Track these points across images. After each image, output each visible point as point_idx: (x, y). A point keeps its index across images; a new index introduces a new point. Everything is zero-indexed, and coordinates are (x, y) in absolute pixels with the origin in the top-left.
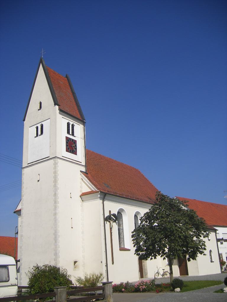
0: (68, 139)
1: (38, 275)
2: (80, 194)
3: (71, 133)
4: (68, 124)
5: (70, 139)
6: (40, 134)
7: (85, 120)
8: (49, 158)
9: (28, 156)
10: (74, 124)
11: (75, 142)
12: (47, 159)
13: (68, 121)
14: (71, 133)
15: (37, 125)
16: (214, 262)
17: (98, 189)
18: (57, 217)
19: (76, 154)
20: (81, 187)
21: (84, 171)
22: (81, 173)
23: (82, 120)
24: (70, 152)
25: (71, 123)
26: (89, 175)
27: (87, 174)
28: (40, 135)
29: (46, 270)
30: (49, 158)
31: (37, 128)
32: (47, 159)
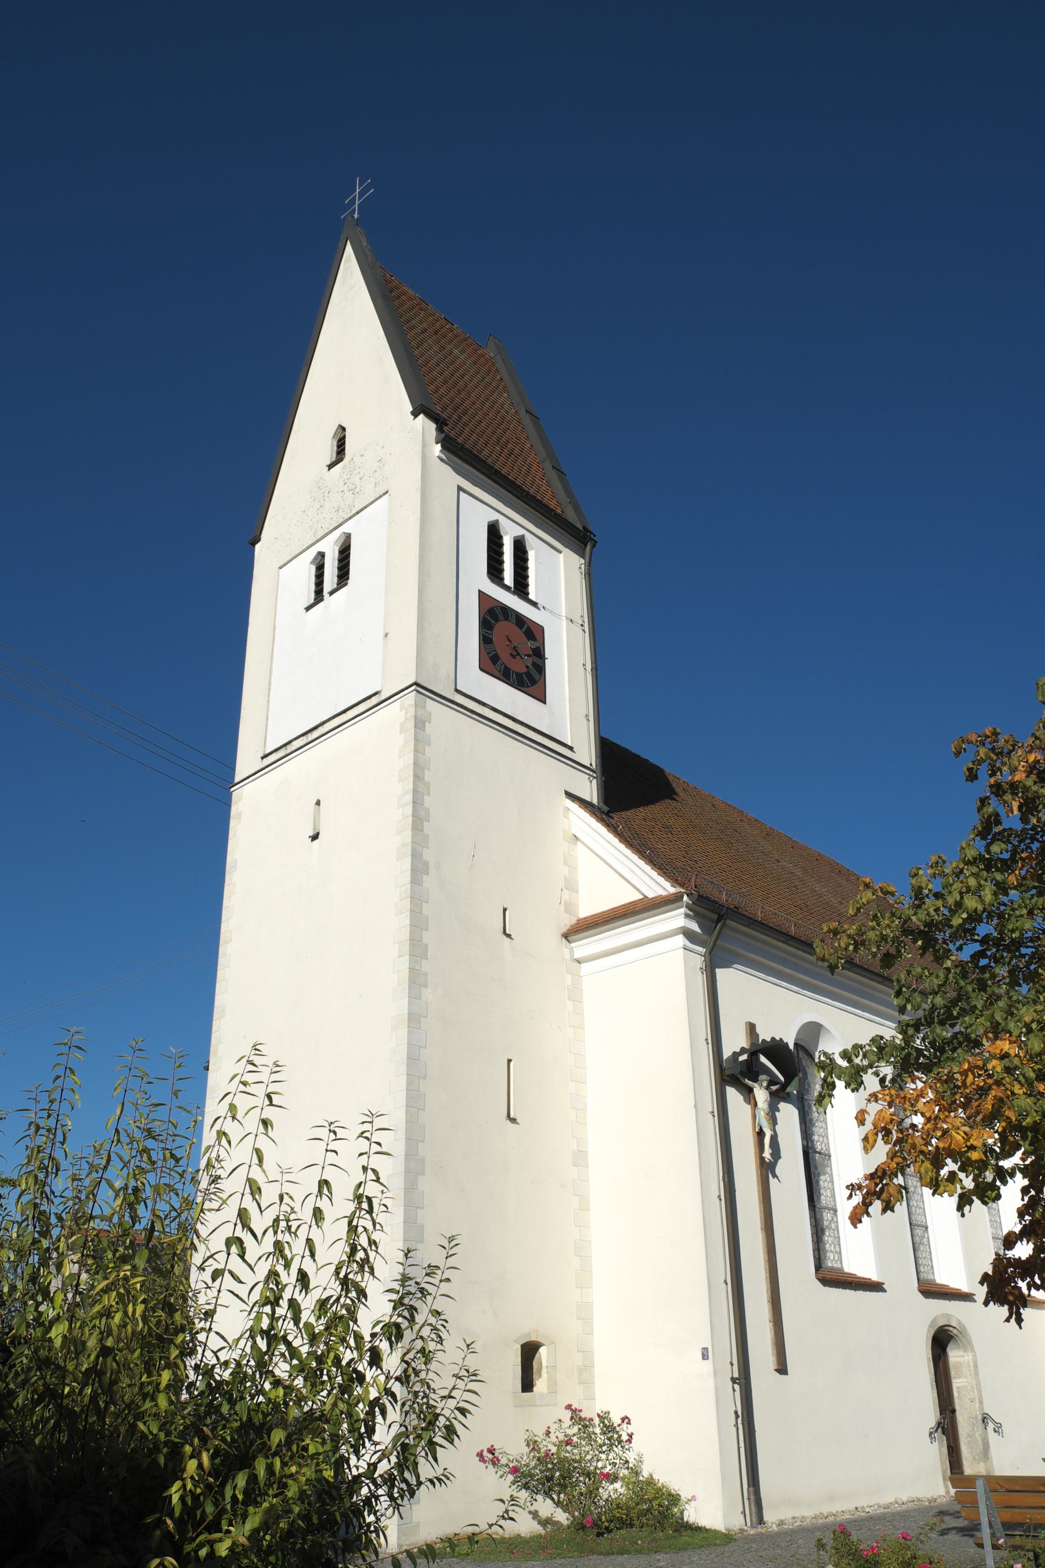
0: (492, 615)
1: (261, 1399)
2: (567, 922)
5: (506, 611)
8: (374, 701)
10: (529, 538)
11: (533, 633)
13: (494, 516)
15: (323, 546)
16: (1021, 1328)
17: (682, 885)
18: (402, 1006)
19: (541, 697)
21: (588, 799)
28: (331, 593)
30: (374, 701)
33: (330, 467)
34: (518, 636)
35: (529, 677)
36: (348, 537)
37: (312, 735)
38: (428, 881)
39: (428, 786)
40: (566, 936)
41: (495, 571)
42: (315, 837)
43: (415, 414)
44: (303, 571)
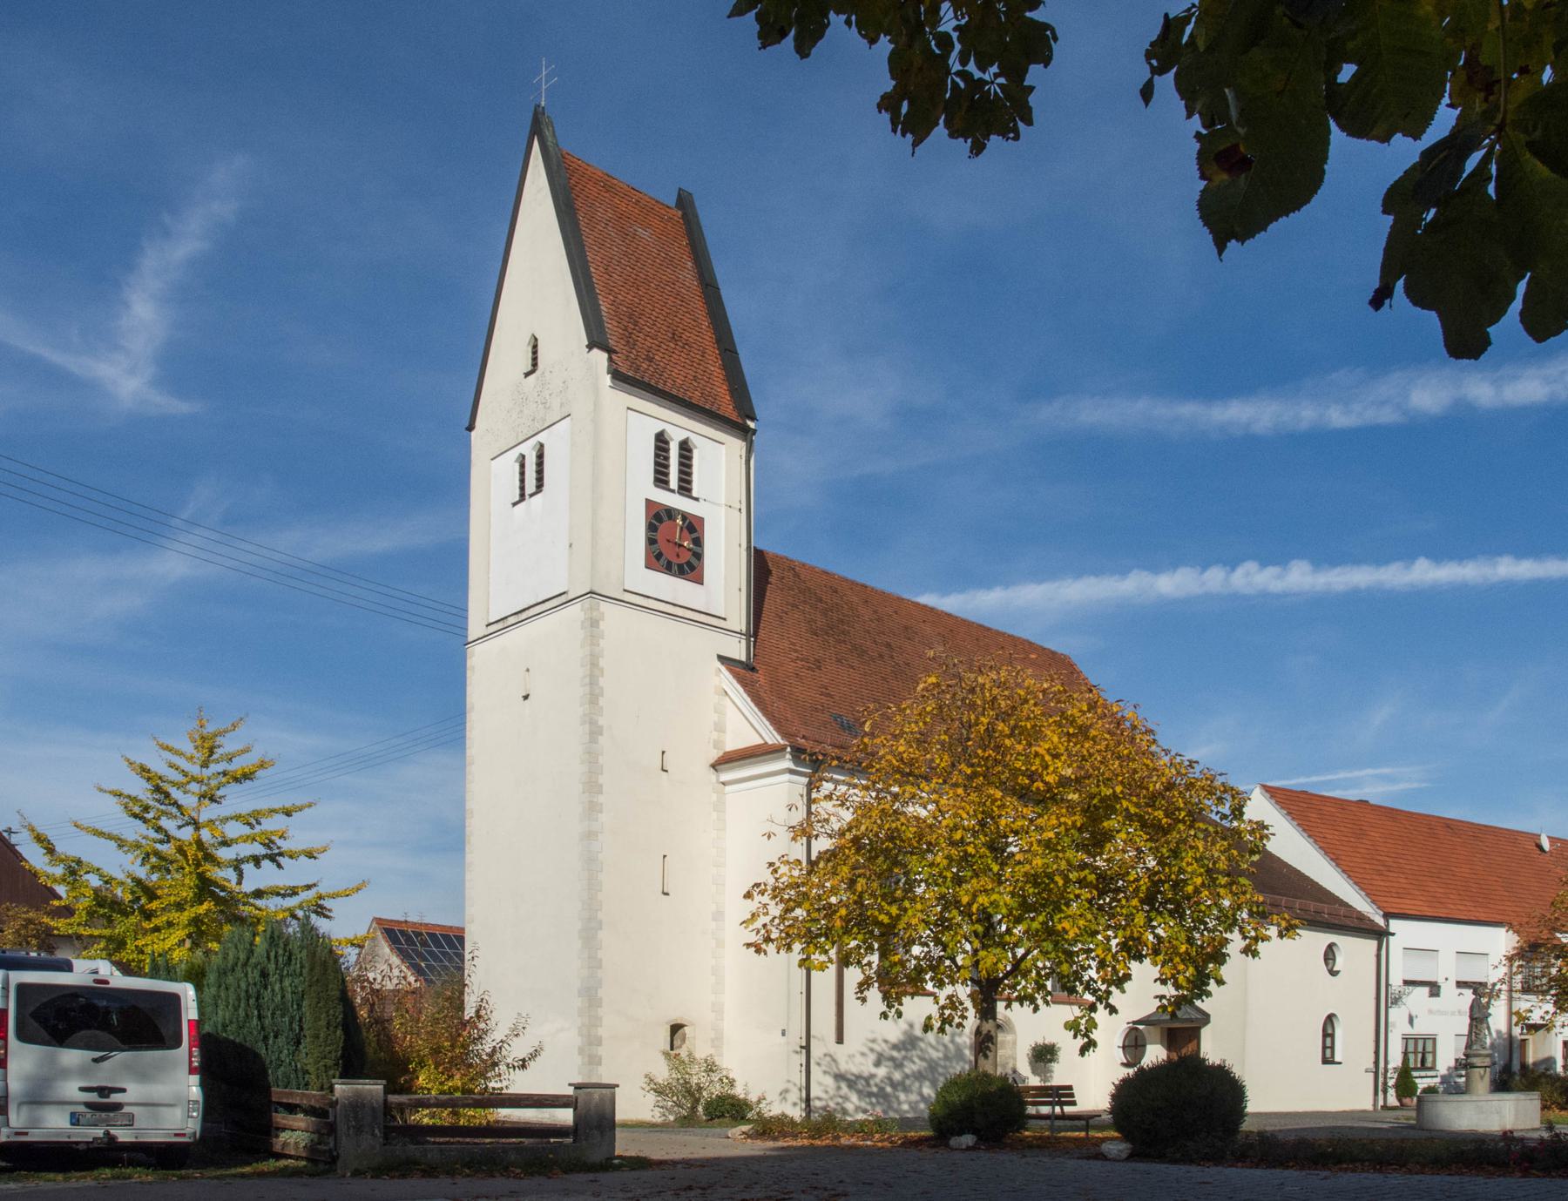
0: (658, 517)
2: (715, 755)
3: (674, 484)
4: (661, 441)
5: (670, 513)
6: (534, 489)
7: (753, 419)
8: (563, 599)
9: (492, 588)
10: (695, 440)
11: (693, 527)
12: (561, 600)
14: (674, 484)
20: (720, 728)
22: (718, 664)
23: (737, 418)
24: (668, 569)
25: (675, 437)
26: (761, 678)
27: (753, 669)
28: (531, 495)
29: (1023, 1127)
30: (563, 599)
31: (522, 461)
32: (561, 600)
33: (527, 375)
34: (669, 553)
35: (689, 567)
36: (542, 446)
37: (523, 615)
38: (603, 740)
39: (602, 670)
40: (713, 766)
41: (661, 479)
42: (526, 697)
43: (590, 347)
44: (509, 464)
